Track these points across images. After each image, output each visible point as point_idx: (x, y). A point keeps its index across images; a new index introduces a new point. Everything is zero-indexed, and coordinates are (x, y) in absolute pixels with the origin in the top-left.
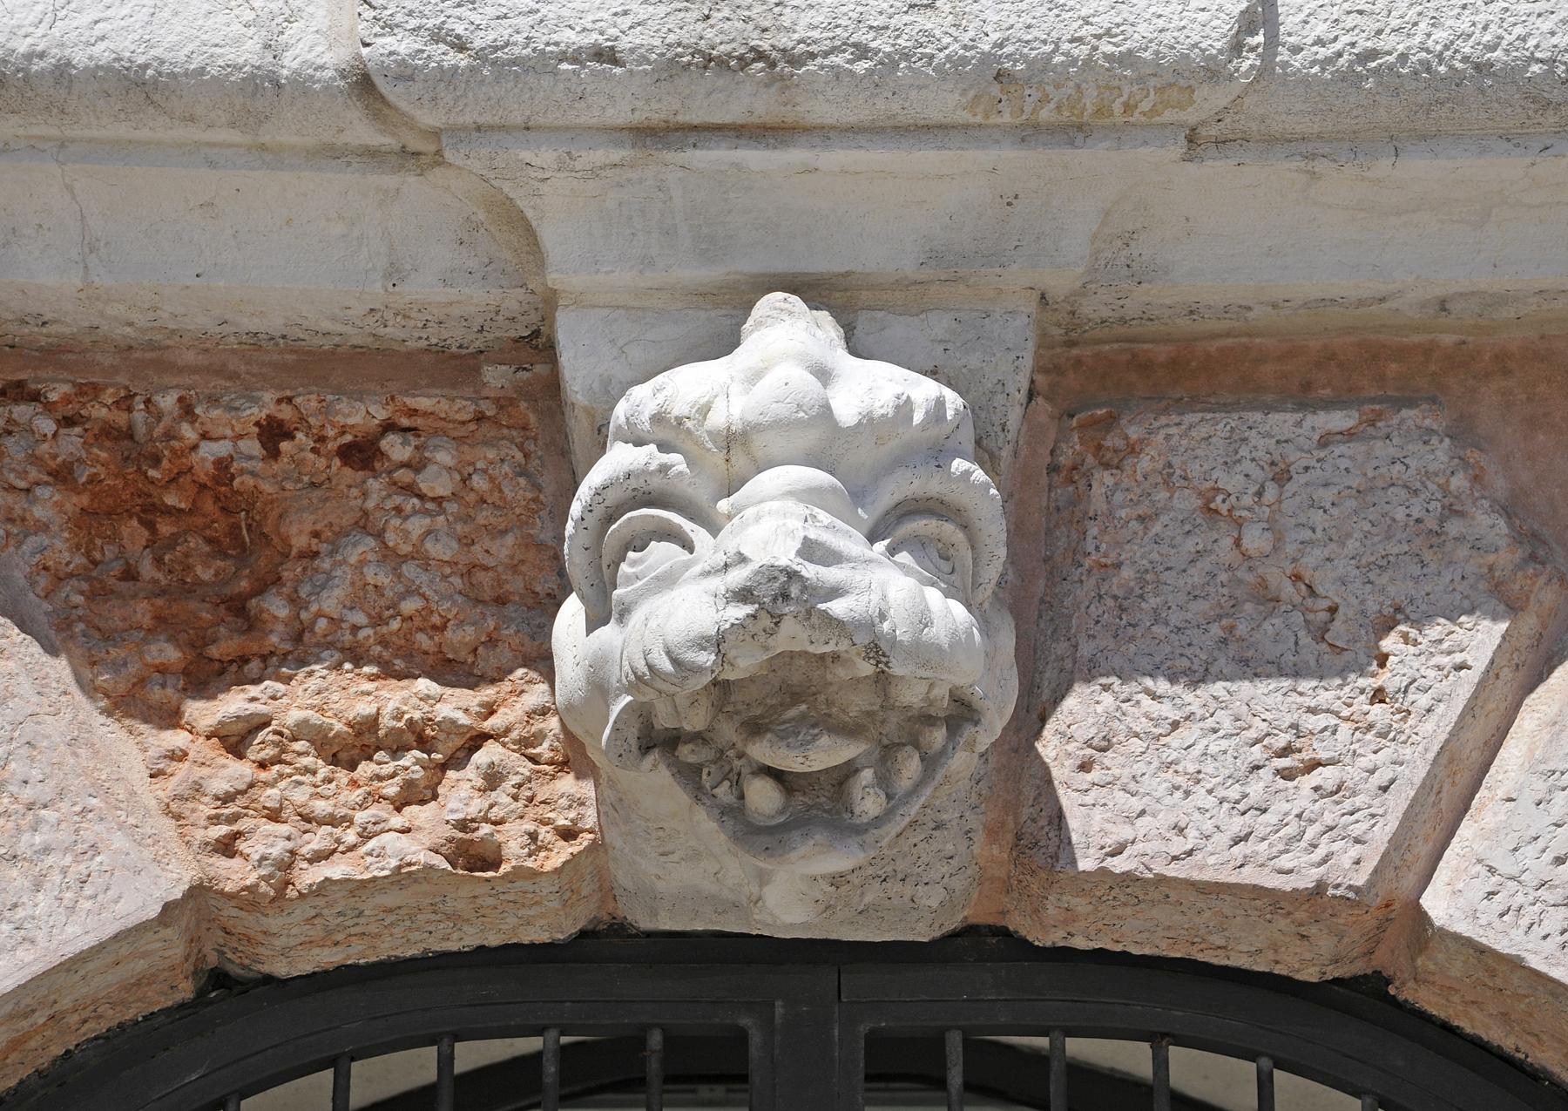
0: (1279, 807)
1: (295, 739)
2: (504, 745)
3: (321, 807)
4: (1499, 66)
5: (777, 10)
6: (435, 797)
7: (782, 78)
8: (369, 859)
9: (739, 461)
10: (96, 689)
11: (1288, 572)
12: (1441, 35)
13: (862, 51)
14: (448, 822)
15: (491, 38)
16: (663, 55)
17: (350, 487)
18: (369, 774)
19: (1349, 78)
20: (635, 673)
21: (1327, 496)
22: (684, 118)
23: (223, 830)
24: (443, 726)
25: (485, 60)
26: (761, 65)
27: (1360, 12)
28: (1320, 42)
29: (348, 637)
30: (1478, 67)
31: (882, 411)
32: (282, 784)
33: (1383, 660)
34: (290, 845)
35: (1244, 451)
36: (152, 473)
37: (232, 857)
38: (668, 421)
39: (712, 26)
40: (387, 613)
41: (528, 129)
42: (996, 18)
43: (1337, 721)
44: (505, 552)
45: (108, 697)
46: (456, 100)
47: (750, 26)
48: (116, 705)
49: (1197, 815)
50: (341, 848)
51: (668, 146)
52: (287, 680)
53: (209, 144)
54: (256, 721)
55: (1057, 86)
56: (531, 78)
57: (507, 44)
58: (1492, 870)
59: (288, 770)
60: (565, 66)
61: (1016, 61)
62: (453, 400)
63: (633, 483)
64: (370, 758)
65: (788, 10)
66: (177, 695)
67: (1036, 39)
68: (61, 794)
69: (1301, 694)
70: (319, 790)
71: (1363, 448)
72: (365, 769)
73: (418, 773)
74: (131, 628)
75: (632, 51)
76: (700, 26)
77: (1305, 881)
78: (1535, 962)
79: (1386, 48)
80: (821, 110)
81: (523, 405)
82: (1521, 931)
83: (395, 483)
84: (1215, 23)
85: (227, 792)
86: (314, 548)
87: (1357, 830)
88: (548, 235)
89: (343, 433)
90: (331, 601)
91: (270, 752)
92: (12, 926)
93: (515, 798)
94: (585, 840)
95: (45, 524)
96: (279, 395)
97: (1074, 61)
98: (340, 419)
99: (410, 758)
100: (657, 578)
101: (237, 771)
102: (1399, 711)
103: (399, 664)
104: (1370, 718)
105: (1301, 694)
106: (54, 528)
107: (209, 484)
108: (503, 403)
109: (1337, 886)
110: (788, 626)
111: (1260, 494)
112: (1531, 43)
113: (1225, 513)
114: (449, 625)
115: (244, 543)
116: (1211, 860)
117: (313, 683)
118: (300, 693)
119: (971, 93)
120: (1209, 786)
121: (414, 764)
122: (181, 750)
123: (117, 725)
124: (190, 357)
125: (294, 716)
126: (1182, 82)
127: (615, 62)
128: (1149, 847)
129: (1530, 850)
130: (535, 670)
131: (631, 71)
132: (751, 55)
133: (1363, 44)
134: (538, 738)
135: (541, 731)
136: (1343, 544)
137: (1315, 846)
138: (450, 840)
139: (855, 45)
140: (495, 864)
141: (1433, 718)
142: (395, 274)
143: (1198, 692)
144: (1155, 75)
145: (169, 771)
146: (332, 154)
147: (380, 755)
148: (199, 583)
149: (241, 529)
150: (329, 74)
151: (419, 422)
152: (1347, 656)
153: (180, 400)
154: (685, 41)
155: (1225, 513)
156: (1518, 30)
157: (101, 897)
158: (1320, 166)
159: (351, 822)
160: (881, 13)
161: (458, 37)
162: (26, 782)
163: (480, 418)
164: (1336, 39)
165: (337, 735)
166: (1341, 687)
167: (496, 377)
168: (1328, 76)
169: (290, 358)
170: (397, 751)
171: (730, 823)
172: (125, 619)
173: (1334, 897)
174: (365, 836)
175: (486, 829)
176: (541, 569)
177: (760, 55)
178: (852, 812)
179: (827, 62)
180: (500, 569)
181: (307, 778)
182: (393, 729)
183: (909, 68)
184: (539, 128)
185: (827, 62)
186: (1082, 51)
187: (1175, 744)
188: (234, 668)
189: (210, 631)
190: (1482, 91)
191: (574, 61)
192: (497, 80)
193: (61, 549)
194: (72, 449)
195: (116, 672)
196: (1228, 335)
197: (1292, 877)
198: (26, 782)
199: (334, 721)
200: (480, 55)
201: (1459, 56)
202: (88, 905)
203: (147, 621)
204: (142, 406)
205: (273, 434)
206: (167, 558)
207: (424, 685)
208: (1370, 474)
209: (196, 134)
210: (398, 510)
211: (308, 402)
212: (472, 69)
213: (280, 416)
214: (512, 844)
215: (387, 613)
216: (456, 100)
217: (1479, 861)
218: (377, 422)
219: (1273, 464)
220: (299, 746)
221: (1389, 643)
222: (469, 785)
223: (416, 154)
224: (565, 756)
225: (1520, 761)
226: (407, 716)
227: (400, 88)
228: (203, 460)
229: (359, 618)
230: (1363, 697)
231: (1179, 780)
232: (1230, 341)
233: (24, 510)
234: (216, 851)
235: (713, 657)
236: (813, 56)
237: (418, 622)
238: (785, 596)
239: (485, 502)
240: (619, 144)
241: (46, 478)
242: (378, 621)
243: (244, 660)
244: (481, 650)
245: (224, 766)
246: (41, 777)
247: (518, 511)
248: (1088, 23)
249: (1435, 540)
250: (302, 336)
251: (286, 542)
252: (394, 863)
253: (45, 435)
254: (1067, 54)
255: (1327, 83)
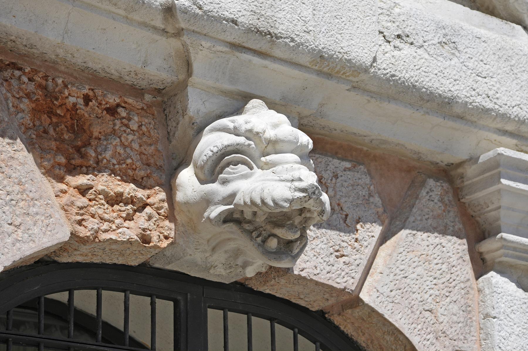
0: (336, 265)
1: (100, 194)
2: (152, 208)
3: (106, 216)
4: (417, 87)
5: (275, 22)
6: (133, 219)
7: (273, 41)
8: (120, 235)
9: (270, 148)
10: (41, 166)
11: (337, 203)
12: (407, 75)
13: (293, 40)
14: (140, 228)
15: (208, 8)
16: (248, 26)
17: (109, 121)
18: (117, 209)
19: (388, 80)
20: (244, 202)
21: (346, 184)
22: (245, 45)
23: (79, 218)
24: (139, 199)
25: (206, 14)
26: (269, 36)
27: (392, 64)
28: (384, 69)
29: (112, 167)
30: (413, 86)
31: (305, 143)
32: (96, 207)
33: (357, 230)
34: (98, 226)
35: (328, 168)
36: (55, 102)
37: (81, 226)
38: (253, 132)
39: (260, 22)
40: (122, 162)
41: (205, 35)
42: (323, 41)
43: (348, 245)
44: (151, 151)
45: (45, 169)
46: (194, 22)
47: (269, 25)
48: (46, 172)
49: (319, 264)
50: (111, 230)
51: (238, 51)
52: (96, 176)
53: (114, 13)
54: (90, 186)
55: (332, 63)
56: (215, 23)
57: (212, 11)
58: (378, 291)
59: (97, 203)
60: (224, 22)
61: (326, 54)
62: (137, 102)
63: (238, 147)
64: (118, 204)
65: (277, 23)
66: (64, 173)
67: (331, 49)
68: (41, 197)
69: (341, 236)
70: (105, 211)
71: (353, 174)
72: (116, 207)
73: (131, 212)
74: (50, 149)
75: (241, 23)
76: (257, 21)
77: (341, 286)
78: (386, 316)
79: (397, 75)
80: (277, 53)
81: (154, 108)
82: (384, 308)
83: (122, 123)
84: (369, 58)
85: (82, 206)
86: (100, 137)
87: (353, 275)
88: (196, 66)
89: (106, 104)
90: (108, 154)
91: (93, 197)
92: (28, 235)
93: (154, 224)
94: (170, 240)
95: (23, 110)
96: (89, 87)
97: (338, 58)
98: (107, 100)
99: (129, 207)
100: (242, 175)
101: (82, 201)
102: (360, 245)
103: (125, 178)
104: (355, 246)
105: (341, 236)
106: (26, 112)
107: (70, 110)
108: (149, 106)
109: (348, 289)
110: (311, 201)
111: (331, 180)
112: (424, 83)
113: (324, 183)
114: (137, 169)
115: (75, 129)
116: (323, 277)
117: (104, 178)
118: (101, 181)
119: (313, 59)
120: (322, 257)
121: (131, 209)
122: (65, 190)
123: (45, 178)
124: (63, 68)
125: (100, 187)
126: (359, 71)
127: (236, 24)
128: (310, 271)
129: (386, 287)
130: (162, 188)
131: (239, 28)
132: (268, 33)
133: (393, 73)
134: (162, 208)
135: (162, 206)
136: (349, 198)
137: (344, 277)
138: (141, 233)
139: (291, 38)
140: (149, 243)
141: (368, 248)
142: (145, 64)
143: (319, 231)
144: (354, 67)
145: (60, 195)
146: (144, 25)
147: (121, 204)
148: (65, 139)
149: (74, 125)
150: (158, 4)
151: (127, 106)
152: (350, 228)
153: (63, 81)
154: (254, 24)
155: (324, 183)
156: (422, 79)
157: (52, 231)
158: (373, 100)
159: (114, 223)
160: (298, 31)
161: (200, 5)
162: (31, 191)
163: (142, 109)
164: (387, 69)
165: (111, 196)
166: (349, 236)
167: (148, 98)
168: (384, 78)
169: (90, 76)
170: (126, 204)
171: (261, 249)
172: (48, 146)
173: (347, 292)
174: (118, 227)
175: (149, 232)
176: (159, 158)
177: (270, 34)
178: (292, 252)
179: (284, 40)
180: (148, 155)
181: (102, 207)
182: (127, 197)
183: (302, 48)
184: (208, 36)
185: (284, 40)
186: (340, 56)
187: (314, 244)
188: (79, 168)
189: (72, 155)
190: (412, 92)
191: (227, 21)
192: (207, 20)
193: (28, 119)
194: (31, 88)
195: (48, 162)
196: (322, 135)
197: (339, 285)
198: (31, 191)
199: (111, 191)
200: (205, 12)
201: (410, 82)
202: (49, 233)
203: (55, 148)
204: (51, 81)
205: (87, 99)
206: (57, 129)
207: (132, 186)
208: (354, 181)
209: (113, 9)
210: (125, 131)
211: (99, 92)
212: (202, 16)
213: (89, 94)
214: (154, 238)
215: (122, 162)
216: (194, 22)
217: (375, 288)
218: (116, 103)
219: (334, 173)
220: (101, 197)
221: (358, 226)
222: (144, 218)
223: (167, 32)
224: (167, 215)
225: (383, 263)
226: (131, 194)
227: (182, 15)
228: (69, 102)
229: (115, 162)
230: (353, 240)
231: (315, 254)
232: (320, 136)
233: (17, 104)
234: (77, 223)
235: (289, 205)
236: (282, 38)
237: (129, 166)
238: (314, 193)
239: (144, 134)
240: (227, 47)
241: (25, 96)
242: (119, 163)
243: (81, 167)
244: (145, 178)
245: (80, 198)
246: (35, 191)
247: (154, 139)
248: (342, 49)
249: (367, 202)
250: (100, 72)
251: (91, 133)
252: (128, 237)
253: (25, 82)
254: (337, 56)
255: (383, 80)
